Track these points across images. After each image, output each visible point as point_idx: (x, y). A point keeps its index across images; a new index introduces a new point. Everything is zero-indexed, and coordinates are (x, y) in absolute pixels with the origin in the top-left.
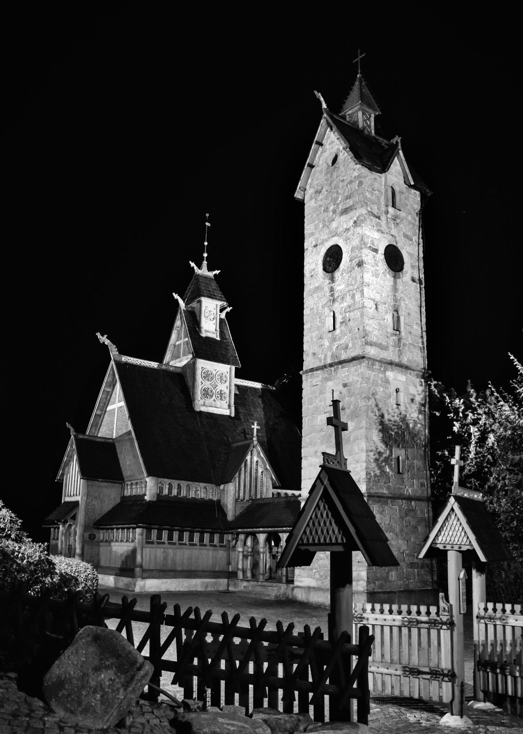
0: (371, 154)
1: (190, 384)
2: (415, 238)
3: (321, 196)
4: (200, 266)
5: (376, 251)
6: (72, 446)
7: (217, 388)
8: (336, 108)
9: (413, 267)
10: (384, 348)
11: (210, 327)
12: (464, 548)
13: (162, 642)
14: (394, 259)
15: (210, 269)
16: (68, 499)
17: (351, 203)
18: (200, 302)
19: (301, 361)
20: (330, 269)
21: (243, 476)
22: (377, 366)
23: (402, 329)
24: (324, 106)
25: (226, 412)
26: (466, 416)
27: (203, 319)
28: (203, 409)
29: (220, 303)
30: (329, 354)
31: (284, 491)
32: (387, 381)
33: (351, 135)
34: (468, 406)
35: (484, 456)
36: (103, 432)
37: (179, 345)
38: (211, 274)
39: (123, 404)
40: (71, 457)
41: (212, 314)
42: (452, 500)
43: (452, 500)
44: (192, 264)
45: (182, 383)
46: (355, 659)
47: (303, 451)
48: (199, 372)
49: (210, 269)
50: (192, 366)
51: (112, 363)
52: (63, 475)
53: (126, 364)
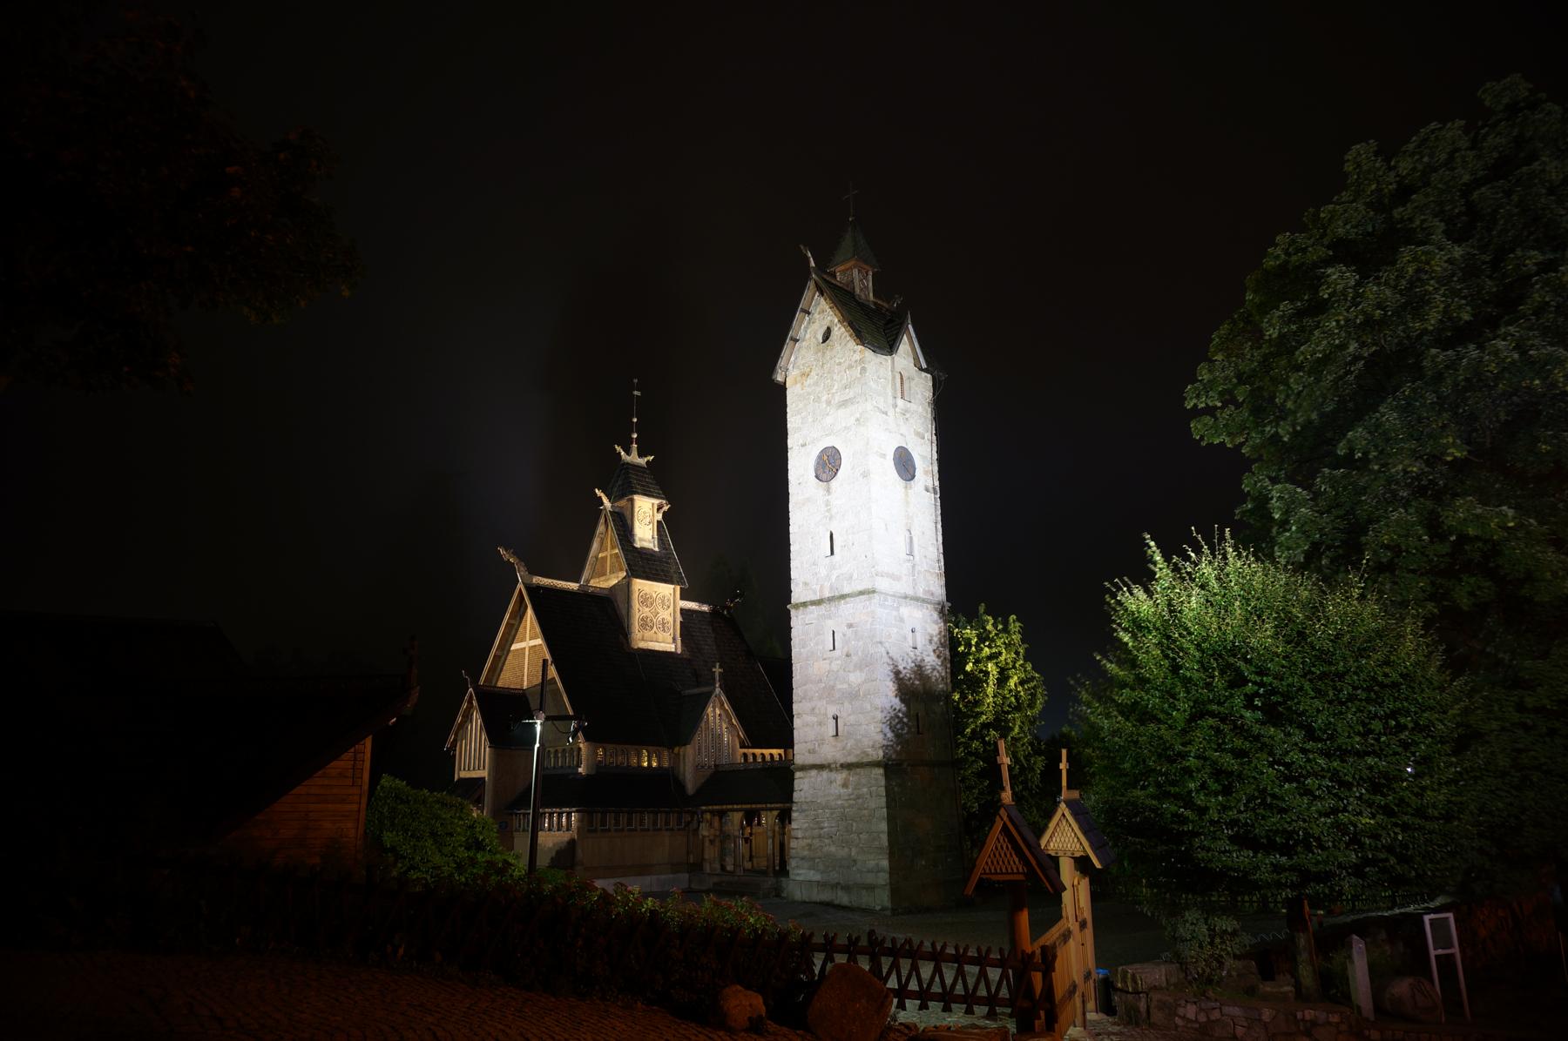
0: (877, 331)
1: (624, 612)
2: (928, 435)
3: (809, 381)
4: (628, 452)
5: (883, 456)
6: (470, 702)
7: (659, 614)
8: (822, 266)
9: (926, 473)
10: (896, 578)
11: (645, 533)
12: (1077, 855)
13: (885, 971)
14: (904, 464)
15: (640, 455)
16: (464, 775)
17: (851, 395)
18: (632, 501)
19: (788, 592)
20: (824, 477)
21: (700, 737)
22: (890, 602)
23: (916, 553)
24: (813, 264)
25: (671, 648)
26: (980, 650)
27: (637, 524)
28: (642, 645)
29: (657, 502)
30: (827, 585)
31: (758, 751)
32: (902, 620)
33: (845, 301)
34: (983, 638)
35: (1004, 697)
36: (506, 680)
37: (604, 559)
38: (642, 461)
39: (539, 641)
40: (468, 717)
41: (646, 515)
42: (1063, 805)
43: (1063, 805)
44: (618, 448)
45: (610, 613)
46: (1037, 978)
47: (795, 707)
48: (635, 596)
49: (640, 455)
50: (625, 587)
51: (520, 586)
52: (455, 740)
53: (539, 587)
